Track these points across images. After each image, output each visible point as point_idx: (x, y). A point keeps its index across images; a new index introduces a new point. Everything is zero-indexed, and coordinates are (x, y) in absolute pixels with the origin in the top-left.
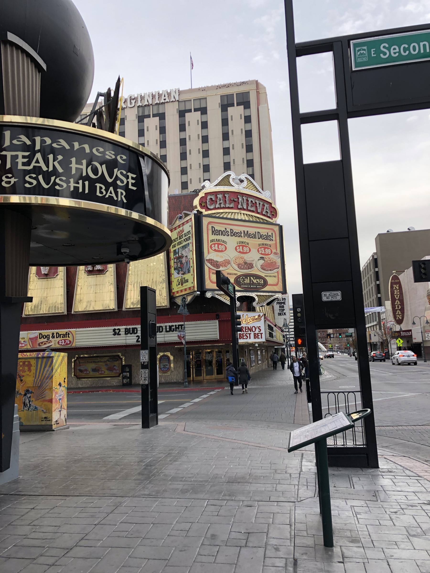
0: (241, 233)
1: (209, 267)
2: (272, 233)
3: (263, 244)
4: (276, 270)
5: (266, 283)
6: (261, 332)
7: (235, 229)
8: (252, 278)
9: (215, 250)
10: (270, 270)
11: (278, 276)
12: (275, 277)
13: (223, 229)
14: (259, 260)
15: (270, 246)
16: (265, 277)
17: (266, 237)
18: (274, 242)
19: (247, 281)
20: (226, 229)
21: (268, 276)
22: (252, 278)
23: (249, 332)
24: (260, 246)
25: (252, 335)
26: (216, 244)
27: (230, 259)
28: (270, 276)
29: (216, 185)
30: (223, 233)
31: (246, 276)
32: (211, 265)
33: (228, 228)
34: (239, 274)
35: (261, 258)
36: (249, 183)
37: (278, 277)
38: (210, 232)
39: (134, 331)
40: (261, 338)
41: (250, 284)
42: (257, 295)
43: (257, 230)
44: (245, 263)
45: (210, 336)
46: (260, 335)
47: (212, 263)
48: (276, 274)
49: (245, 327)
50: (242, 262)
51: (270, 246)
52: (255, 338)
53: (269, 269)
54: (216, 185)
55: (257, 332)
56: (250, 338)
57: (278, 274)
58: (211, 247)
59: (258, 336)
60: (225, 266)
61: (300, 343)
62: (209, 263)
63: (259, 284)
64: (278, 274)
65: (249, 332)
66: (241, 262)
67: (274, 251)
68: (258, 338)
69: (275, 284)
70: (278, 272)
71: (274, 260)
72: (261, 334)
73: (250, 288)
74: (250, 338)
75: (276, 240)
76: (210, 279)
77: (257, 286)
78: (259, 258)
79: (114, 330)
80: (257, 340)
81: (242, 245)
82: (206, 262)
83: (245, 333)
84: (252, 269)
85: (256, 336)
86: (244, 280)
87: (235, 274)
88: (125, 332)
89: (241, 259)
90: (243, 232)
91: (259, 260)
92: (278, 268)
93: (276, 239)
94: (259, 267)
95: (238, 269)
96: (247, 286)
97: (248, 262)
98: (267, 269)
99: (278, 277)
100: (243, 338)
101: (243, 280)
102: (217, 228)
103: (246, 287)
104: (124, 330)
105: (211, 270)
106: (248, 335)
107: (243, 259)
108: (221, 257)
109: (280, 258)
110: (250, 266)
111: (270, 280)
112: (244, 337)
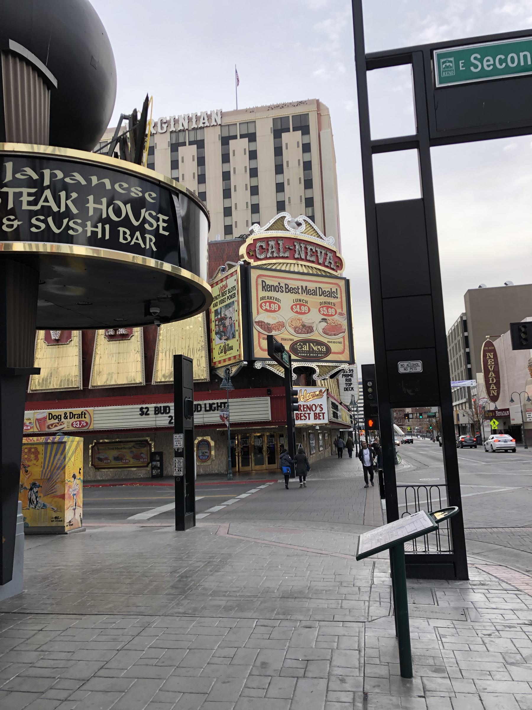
0: (298, 289)
1: (258, 331)
2: (337, 289)
3: (325, 303)
4: (341, 335)
5: (329, 351)
6: (322, 412)
7: (291, 284)
8: (311, 344)
9: (266, 310)
10: (335, 335)
11: (344, 342)
12: (340, 343)
13: (276, 284)
14: (320, 322)
15: (334, 305)
16: (328, 344)
17: (329, 294)
18: (339, 300)
19: (306, 348)
20: (279, 283)
21: (331, 342)
22: (311, 344)
23: (308, 412)
24: (322, 305)
25: (312, 416)
26: (268, 302)
27: (284, 321)
28: (334, 342)
29: (268, 230)
30: (275, 289)
31: (305, 342)
32: (261, 328)
33: (283, 283)
34: (296, 339)
35: (322, 319)
36: (308, 226)
37: (344, 344)
38: (260, 287)
39: (166, 410)
40: (324, 419)
41: (309, 352)
42: (318, 366)
43: (318, 285)
44: (304, 326)
45: (260, 416)
46: (321, 415)
47: (263, 326)
48: (342, 340)
49: (304, 405)
50: (300, 324)
51: (334, 305)
52: (315, 419)
53: (333, 333)
54: (268, 230)
55: (318, 411)
56: (309, 419)
57: (344, 340)
58: (261, 306)
59: (319, 416)
60: (279, 330)
61: (371, 425)
62: (259, 326)
63: (320, 352)
64: (344, 340)
65: (308, 412)
66: (299, 324)
67: (339, 311)
68: (319, 419)
69: (340, 351)
70: (344, 337)
71: (339, 323)
72: (323, 413)
73: (310, 356)
74: (309, 419)
75: (341, 298)
76: (260, 346)
77: (318, 354)
78: (320, 320)
79: (141, 409)
80: (318, 422)
81: (300, 303)
82: (255, 324)
83: (303, 413)
84: (312, 334)
85: (317, 416)
86: (302, 348)
87: (291, 340)
88: (155, 411)
89: (298, 321)
90: (300, 288)
91: (320, 322)
92: (344, 332)
93: (341, 296)
94: (321, 331)
95: (294, 334)
96: (305, 355)
97: (307, 325)
98: (330, 333)
99: (344, 344)
100: (301, 419)
101: (300, 347)
102: (269, 282)
103: (304, 356)
104: (153, 409)
105: (261, 334)
106: (307, 415)
107: (301, 321)
108: (274, 318)
109: (346, 320)
110: (309, 329)
111: (334, 347)
112: (302, 418)
